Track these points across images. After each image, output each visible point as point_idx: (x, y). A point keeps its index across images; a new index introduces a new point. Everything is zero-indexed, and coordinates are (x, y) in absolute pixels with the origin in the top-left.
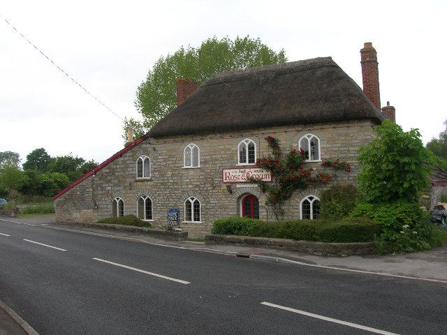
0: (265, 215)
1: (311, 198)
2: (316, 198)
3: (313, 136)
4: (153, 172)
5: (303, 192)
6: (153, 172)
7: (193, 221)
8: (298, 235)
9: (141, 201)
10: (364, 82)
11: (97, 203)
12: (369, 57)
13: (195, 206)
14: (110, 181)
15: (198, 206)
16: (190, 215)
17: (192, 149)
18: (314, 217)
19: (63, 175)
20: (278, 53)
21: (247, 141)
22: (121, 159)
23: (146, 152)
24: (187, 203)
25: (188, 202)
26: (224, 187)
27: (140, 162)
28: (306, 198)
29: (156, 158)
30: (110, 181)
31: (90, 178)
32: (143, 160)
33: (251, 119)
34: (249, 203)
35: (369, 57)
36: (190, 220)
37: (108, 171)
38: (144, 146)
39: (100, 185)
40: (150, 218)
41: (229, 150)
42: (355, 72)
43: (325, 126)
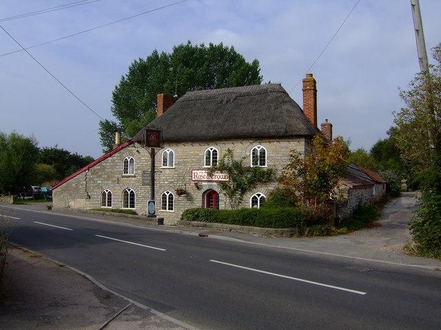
0: (224, 203)
1: (259, 195)
2: (262, 195)
3: (262, 147)
4: (136, 170)
5: (426, 210)
6: (136, 170)
7: (167, 210)
8: (246, 219)
9: (104, 194)
10: (304, 105)
11: (89, 194)
12: (311, 86)
13: (169, 198)
14: (100, 176)
15: (172, 198)
16: (166, 205)
17: (168, 153)
18: (260, 205)
19: (49, 166)
20: (230, 48)
21: (212, 149)
22: (110, 158)
23: (131, 153)
24: (253, 198)
25: (164, 195)
26: (193, 184)
27: (126, 162)
28: (255, 195)
29: (139, 159)
30: (100, 176)
31: (84, 173)
32: (129, 160)
33: (216, 132)
34: (211, 196)
35: (311, 86)
36: (166, 209)
37: (99, 167)
38: (130, 149)
39: (91, 179)
40: (111, 206)
41: (198, 155)
42: (297, 96)
43: (271, 140)
